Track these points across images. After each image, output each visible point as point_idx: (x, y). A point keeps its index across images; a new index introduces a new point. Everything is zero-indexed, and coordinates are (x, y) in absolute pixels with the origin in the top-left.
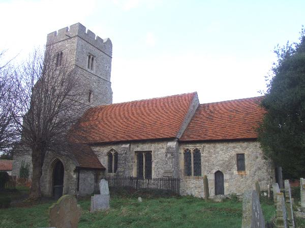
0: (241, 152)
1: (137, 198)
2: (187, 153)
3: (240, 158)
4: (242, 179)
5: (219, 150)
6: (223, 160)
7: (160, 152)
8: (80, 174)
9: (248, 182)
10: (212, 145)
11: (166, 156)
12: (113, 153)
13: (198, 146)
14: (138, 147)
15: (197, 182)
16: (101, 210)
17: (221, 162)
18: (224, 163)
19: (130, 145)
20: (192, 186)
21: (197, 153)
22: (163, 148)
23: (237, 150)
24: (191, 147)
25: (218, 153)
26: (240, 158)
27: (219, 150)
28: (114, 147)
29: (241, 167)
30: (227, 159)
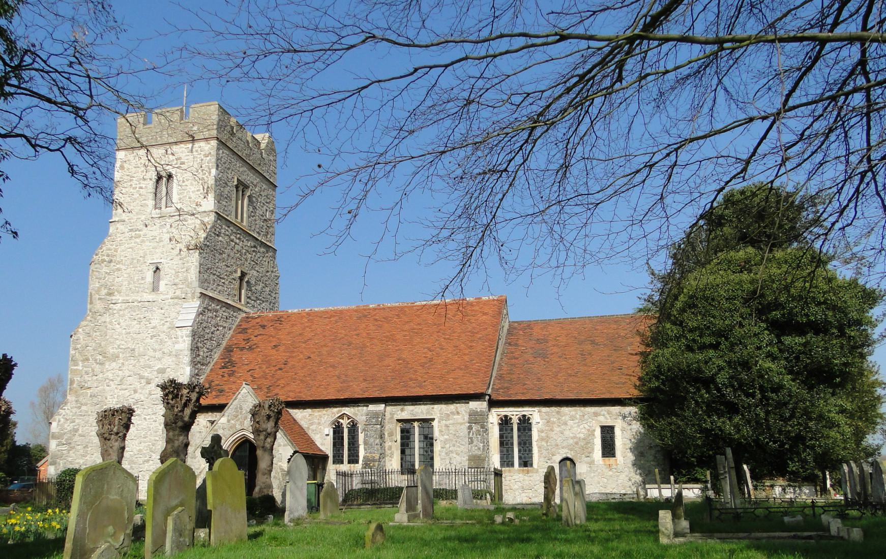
0: (609, 423)
1: (46, 511)
2: (505, 423)
3: (608, 433)
4: (611, 473)
5: (567, 418)
6: (574, 437)
7: (451, 422)
8: (540, 499)
9: (621, 477)
10: (554, 409)
11: (470, 428)
12: (345, 422)
13: (526, 411)
14: (402, 410)
15: (526, 478)
16: (500, 550)
17: (571, 441)
18: (577, 443)
19: (385, 408)
20: (516, 487)
21: (525, 424)
22: (458, 413)
23: (601, 418)
24: (514, 413)
25: (566, 424)
26: (608, 433)
27: (567, 418)
28: (346, 410)
29: (608, 449)
30: (582, 436)
